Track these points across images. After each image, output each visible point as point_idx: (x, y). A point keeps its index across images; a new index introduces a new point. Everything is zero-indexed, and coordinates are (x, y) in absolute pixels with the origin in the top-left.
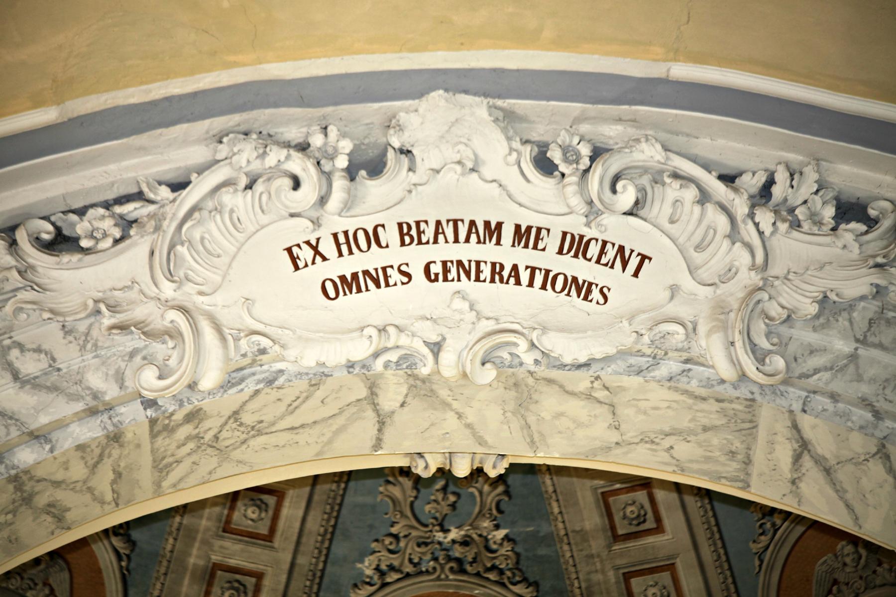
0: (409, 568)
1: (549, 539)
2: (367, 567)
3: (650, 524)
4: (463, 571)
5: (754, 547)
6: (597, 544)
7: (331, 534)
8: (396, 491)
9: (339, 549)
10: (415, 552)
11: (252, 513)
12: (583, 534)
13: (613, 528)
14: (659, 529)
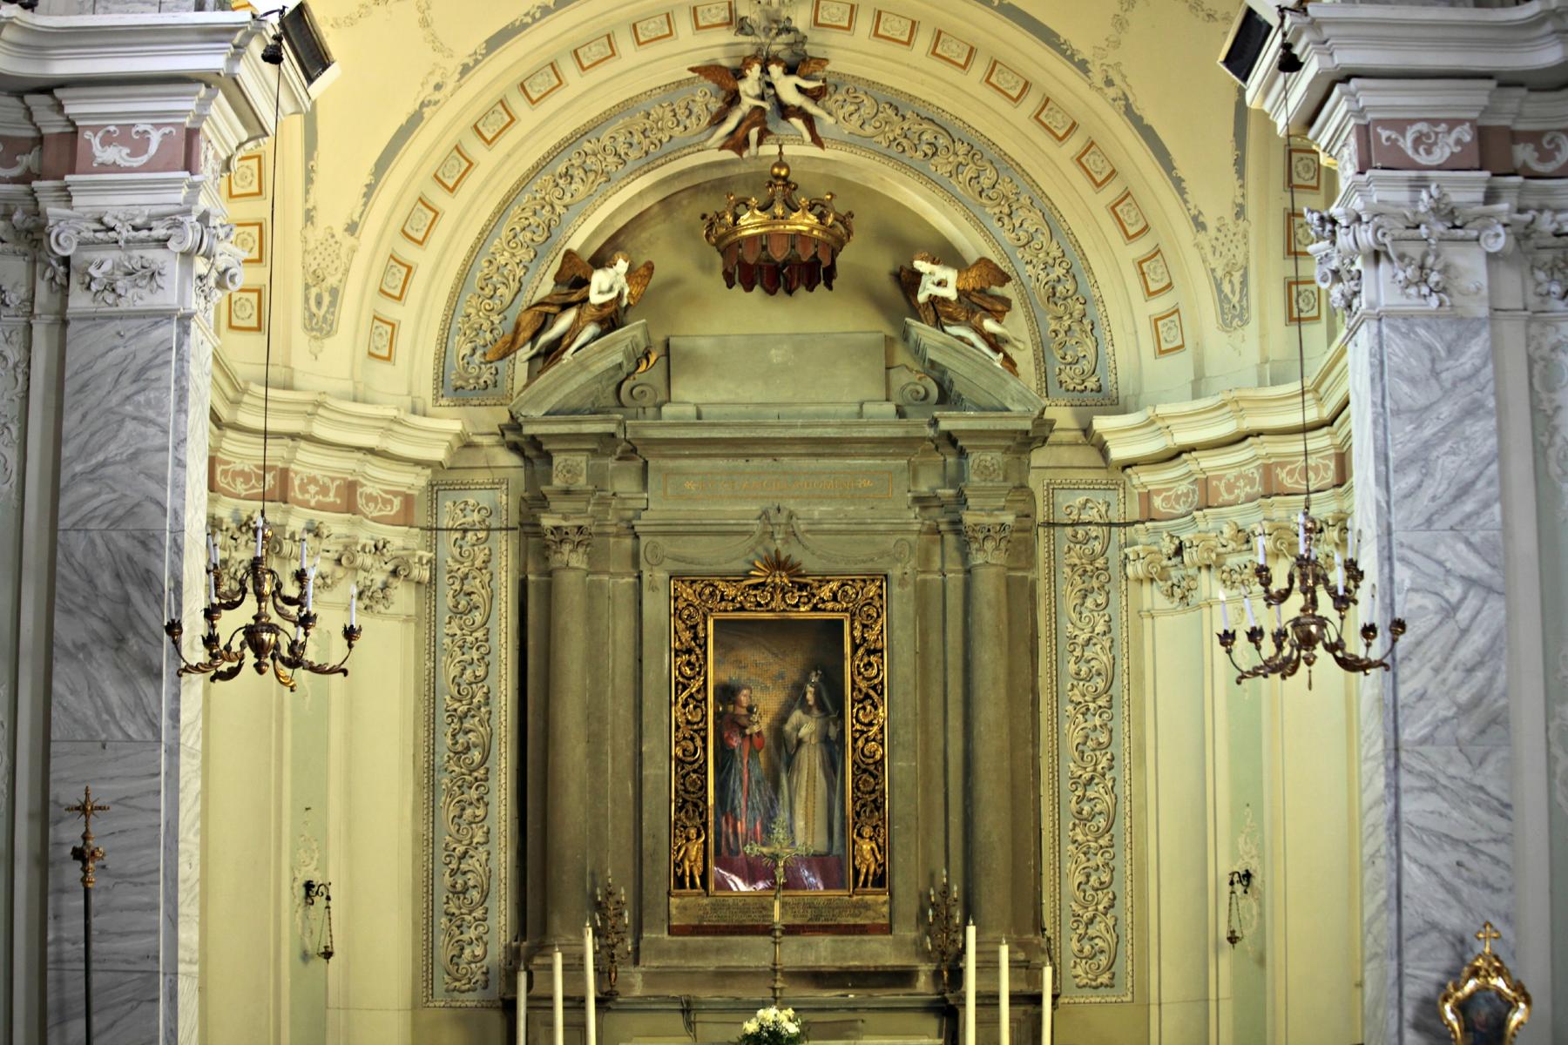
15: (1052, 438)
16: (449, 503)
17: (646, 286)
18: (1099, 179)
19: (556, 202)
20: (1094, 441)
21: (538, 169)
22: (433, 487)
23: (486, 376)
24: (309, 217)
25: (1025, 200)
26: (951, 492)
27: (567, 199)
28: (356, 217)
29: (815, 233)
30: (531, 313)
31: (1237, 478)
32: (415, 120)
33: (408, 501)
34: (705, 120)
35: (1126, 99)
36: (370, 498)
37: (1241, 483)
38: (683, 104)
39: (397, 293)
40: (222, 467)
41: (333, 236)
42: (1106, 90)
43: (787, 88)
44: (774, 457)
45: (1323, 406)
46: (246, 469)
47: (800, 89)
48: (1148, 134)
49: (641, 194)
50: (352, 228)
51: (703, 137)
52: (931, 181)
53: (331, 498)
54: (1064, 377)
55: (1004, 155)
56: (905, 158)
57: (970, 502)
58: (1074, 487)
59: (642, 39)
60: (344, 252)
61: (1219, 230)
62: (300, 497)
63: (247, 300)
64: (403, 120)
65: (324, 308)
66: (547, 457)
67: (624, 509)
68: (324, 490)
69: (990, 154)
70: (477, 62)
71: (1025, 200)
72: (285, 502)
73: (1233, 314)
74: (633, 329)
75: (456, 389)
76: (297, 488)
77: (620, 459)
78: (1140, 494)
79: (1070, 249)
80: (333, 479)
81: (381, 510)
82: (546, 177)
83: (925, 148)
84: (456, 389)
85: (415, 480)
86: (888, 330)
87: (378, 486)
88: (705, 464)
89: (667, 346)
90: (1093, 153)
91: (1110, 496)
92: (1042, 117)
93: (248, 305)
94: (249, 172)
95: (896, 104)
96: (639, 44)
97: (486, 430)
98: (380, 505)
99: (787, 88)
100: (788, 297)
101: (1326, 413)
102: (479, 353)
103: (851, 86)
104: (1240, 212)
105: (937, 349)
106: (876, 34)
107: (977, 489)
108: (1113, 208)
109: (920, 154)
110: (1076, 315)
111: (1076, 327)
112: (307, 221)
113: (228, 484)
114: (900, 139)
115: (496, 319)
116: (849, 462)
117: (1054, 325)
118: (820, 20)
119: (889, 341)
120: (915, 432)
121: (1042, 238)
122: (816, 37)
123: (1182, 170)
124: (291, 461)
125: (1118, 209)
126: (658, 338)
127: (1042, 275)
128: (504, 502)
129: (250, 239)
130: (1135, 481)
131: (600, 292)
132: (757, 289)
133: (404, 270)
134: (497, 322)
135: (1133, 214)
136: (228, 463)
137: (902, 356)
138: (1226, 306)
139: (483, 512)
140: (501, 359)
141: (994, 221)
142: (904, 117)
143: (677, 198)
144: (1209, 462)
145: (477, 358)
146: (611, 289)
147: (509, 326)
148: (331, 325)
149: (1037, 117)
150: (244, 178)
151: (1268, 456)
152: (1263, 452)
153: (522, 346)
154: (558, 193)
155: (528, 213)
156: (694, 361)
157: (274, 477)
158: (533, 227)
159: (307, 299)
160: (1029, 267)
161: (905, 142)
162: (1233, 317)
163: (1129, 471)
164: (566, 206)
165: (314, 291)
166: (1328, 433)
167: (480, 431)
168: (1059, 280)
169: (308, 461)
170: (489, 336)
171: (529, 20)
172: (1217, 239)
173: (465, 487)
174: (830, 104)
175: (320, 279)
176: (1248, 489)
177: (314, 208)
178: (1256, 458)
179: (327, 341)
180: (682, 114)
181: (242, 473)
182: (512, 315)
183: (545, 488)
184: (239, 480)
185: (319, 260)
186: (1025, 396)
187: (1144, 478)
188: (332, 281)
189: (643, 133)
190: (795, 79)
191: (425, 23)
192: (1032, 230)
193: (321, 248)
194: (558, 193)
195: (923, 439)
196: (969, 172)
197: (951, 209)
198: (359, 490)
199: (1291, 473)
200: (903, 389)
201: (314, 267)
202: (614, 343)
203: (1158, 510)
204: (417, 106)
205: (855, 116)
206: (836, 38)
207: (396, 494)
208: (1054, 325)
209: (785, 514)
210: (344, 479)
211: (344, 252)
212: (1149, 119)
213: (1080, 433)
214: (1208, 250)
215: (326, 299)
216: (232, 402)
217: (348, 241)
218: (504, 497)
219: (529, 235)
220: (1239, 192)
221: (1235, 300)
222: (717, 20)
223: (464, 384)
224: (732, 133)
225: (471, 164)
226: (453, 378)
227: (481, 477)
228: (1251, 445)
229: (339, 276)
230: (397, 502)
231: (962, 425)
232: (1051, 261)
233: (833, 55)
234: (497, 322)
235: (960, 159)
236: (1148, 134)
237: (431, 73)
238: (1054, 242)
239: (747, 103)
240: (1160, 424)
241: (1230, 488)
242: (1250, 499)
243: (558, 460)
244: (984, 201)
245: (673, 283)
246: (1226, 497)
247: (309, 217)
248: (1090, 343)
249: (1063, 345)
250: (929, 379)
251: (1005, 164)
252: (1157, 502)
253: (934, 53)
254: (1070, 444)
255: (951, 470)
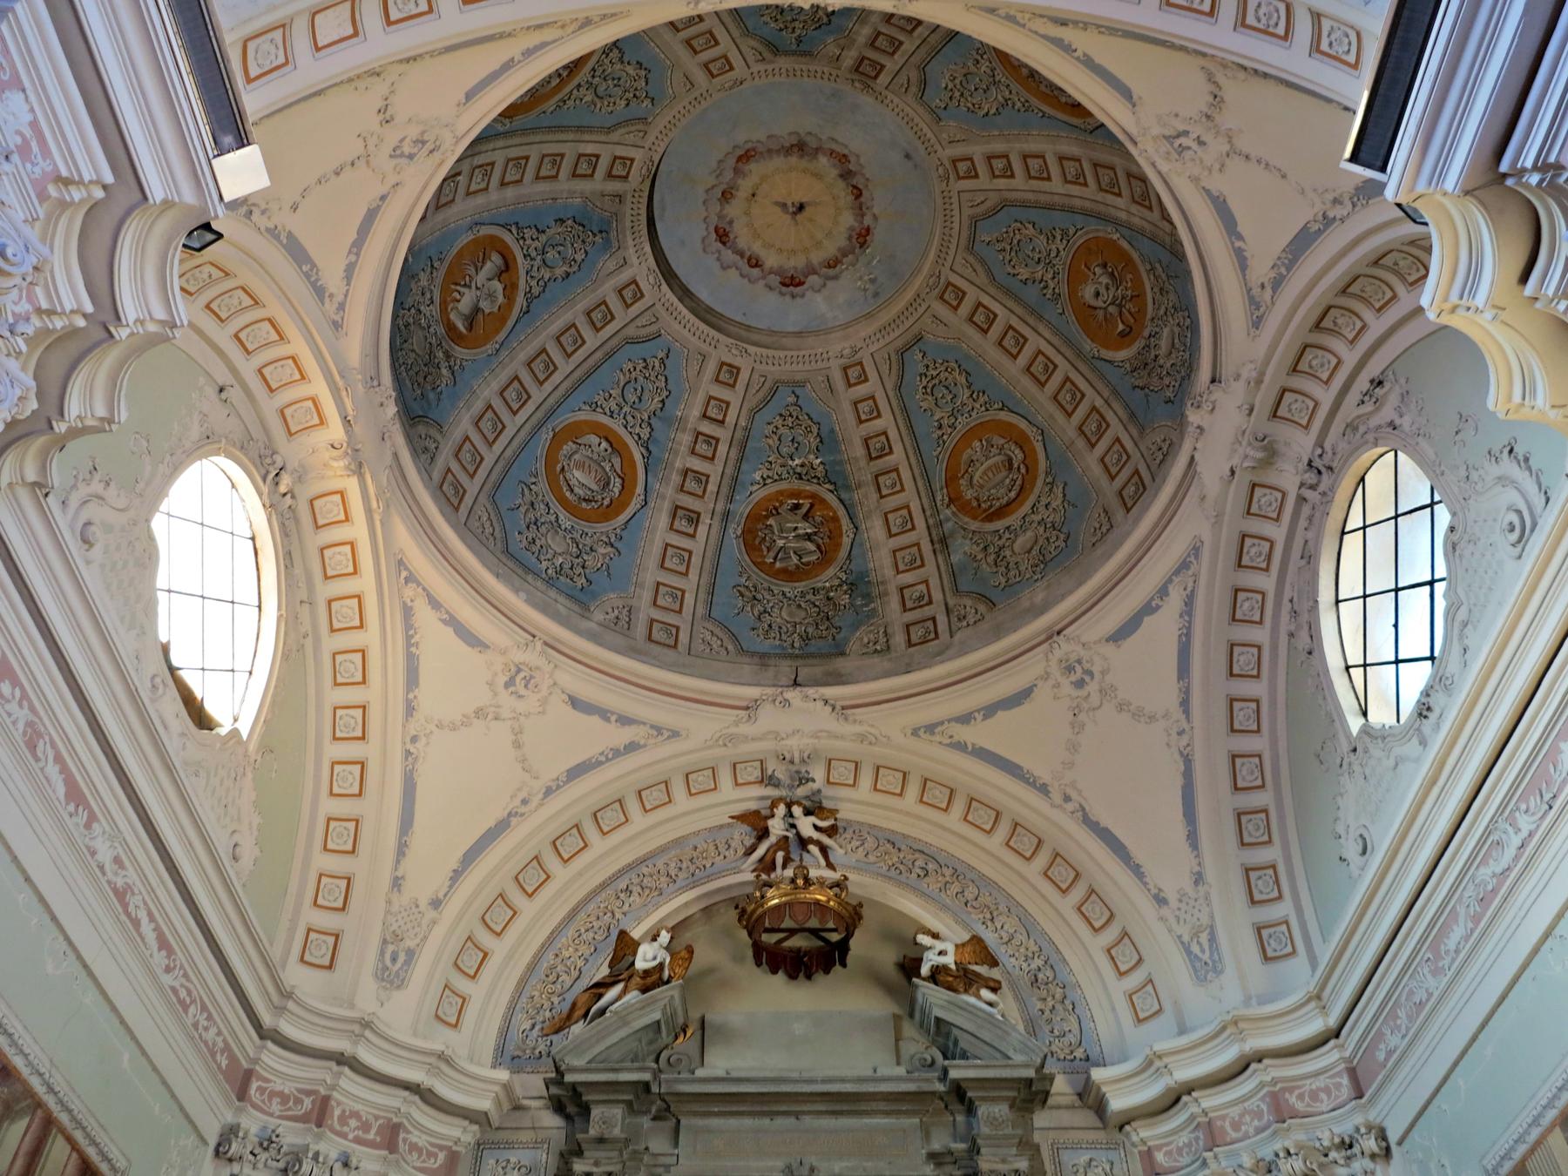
0: (776, 477)
1: (841, 463)
2: (757, 476)
3: (887, 450)
4: (801, 478)
5: (935, 454)
6: (863, 463)
7: (740, 460)
8: (770, 441)
9: (745, 467)
10: (780, 470)
11: (705, 446)
12: (856, 459)
13: (870, 454)
14: (891, 452)
15: (1050, 1101)
16: (492, 1162)
17: (687, 968)
18: (1064, 886)
19: (617, 910)
20: (1091, 1101)
21: (603, 886)
22: (480, 1147)
23: (542, 1047)
24: (397, 883)
25: (1003, 908)
26: (962, 1146)
27: (626, 908)
28: (441, 895)
29: (832, 903)
30: (587, 995)
31: (1242, 1115)
32: (502, 827)
33: (453, 1157)
34: (741, 852)
35: (1083, 809)
36: (414, 1147)
37: (1248, 1118)
38: (724, 841)
39: (472, 972)
40: (260, 1083)
41: (417, 906)
42: (1065, 806)
43: (806, 826)
44: (797, 1115)
45: (1327, 1015)
46: (286, 1091)
47: (816, 827)
48: (1106, 836)
49: (686, 905)
50: (436, 904)
51: (739, 863)
52: (923, 894)
53: (371, 1136)
54: (1054, 1048)
55: (983, 876)
56: (903, 878)
57: (983, 1151)
58: (1076, 1147)
59: (693, 791)
60: (425, 922)
61: (1180, 901)
62: (338, 1127)
63: (324, 942)
64: (492, 823)
65: (398, 965)
66: (585, 1110)
67: (655, 1166)
68: (366, 1127)
69: (970, 875)
70: (558, 787)
71: (1003, 908)
72: (319, 1125)
73: (1206, 968)
74: (673, 988)
75: (513, 1058)
76: (336, 1118)
77: (654, 1119)
78: (1140, 1152)
79: (1045, 945)
80: (377, 1118)
81: (424, 1161)
82: (609, 891)
83: (919, 871)
84: (513, 1058)
85: (460, 1133)
86: (896, 1009)
87: (424, 1137)
88: (733, 1122)
89: (703, 1021)
90: (1058, 865)
91: (1113, 1155)
92: (1011, 843)
93: (324, 947)
94: (346, 833)
95: (892, 841)
96: (691, 795)
97: (535, 1094)
98: (424, 1157)
99: (806, 826)
100: (808, 983)
101: (1332, 1021)
102: (538, 1027)
103: (857, 828)
104: (1199, 879)
105: (942, 1007)
106: (875, 789)
107: (989, 1137)
108: (1079, 909)
109: (914, 875)
110: (1058, 996)
111: (1059, 1007)
112: (394, 886)
113: (263, 1101)
114: (898, 865)
115: (556, 1000)
116: (867, 1121)
117: (1039, 1005)
118: (831, 780)
119: (897, 1018)
120: (926, 1087)
121: (1021, 937)
122: (828, 791)
123: (1139, 856)
124: (333, 1087)
125: (1083, 909)
126: (695, 1015)
127: (1024, 965)
128: (544, 1160)
129: (337, 890)
130: (1135, 1138)
131: (645, 960)
132: (780, 973)
133: (481, 955)
134: (556, 1002)
135: (1097, 909)
136: (267, 1081)
137: (909, 1030)
138: (1198, 965)
139: (523, 1170)
140: (557, 1032)
141: (980, 925)
142: (899, 850)
143: (715, 908)
144: (1210, 1101)
145: (536, 1032)
146: (655, 958)
147: (566, 1006)
148: (403, 980)
149: (1007, 844)
150: (340, 835)
151: (1274, 1082)
152: (1269, 1079)
153: (576, 1022)
154: (619, 903)
155: (592, 918)
156: (727, 1035)
157: (313, 1102)
158: (596, 929)
159: (382, 953)
160: (1013, 960)
161: (901, 867)
162: (1207, 972)
163: (1127, 1128)
164: (624, 914)
165: (390, 948)
166: (1336, 1047)
167: (530, 1095)
168: (1039, 969)
169: (352, 1091)
170: (548, 1014)
171: (603, 758)
172: (1179, 909)
173: (510, 1146)
174: (841, 840)
175: (398, 938)
176: (1256, 1123)
177: (403, 877)
178: (1262, 1085)
179: (396, 994)
180: (722, 848)
181: (281, 1094)
182: (570, 997)
183: (580, 1136)
184: (276, 1100)
185: (401, 922)
186: (1026, 1045)
187: (1144, 1133)
188: (410, 943)
189: (691, 860)
190: (812, 819)
191: (517, 745)
192: (1011, 931)
193: (404, 914)
194: (619, 903)
195: (933, 1093)
196: (955, 888)
197: (941, 914)
198: (402, 1135)
199: (1301, 1097)
200: (912, 1057)
201: (395, 927)
202: (654, 1001)
203: (1161, 1165)
204: (506, 815)
205: (861, 849)
206: (844, 792)
207: (441, 1148)
208: (1039, 1005)
209: (807, 1167)
210: (390, 1120)
211: (425, 922)
212: (1106, 821)
213: (1075, 1098)
214: (1172, 921)
215: (402, 957)
216: (276, 1008)
217: (432, 914)
218: (545, 1156)
219: (591, 934)
220: (1195, 862)
221: (1206, 957)
222: (752, 779)
223: (520, 1054)
224: (761, 860)
225: (548, 877)
226: (511, 1049)
227: (526, 1136)
228: (1255, 1071)
229: (418, 941)
230: (442, 1156)
231: (971, 1074)
232: (1030, 955)
233: (842, 806)
234: (556, 1002)
235: (948, 879)
236: (1106, 836)
237: (519, 789)
238: (1032, 941)
239: (772, 839)
240: (1158, 1063)
241: (1236, 1126)
242: (1259, 1131)
243: (596, 1112)
244: (970, 909)
245: (710, 971)
246: (1234, 1135)
247: (397, 883)
248: (1073, 1019)
249: (1049, 1021)
250: (934, 1049)
251: (983, 881)
252: (1160, 1157)
253: (921, 801)
254: (1067, 1107)
255: (961, 1127)
